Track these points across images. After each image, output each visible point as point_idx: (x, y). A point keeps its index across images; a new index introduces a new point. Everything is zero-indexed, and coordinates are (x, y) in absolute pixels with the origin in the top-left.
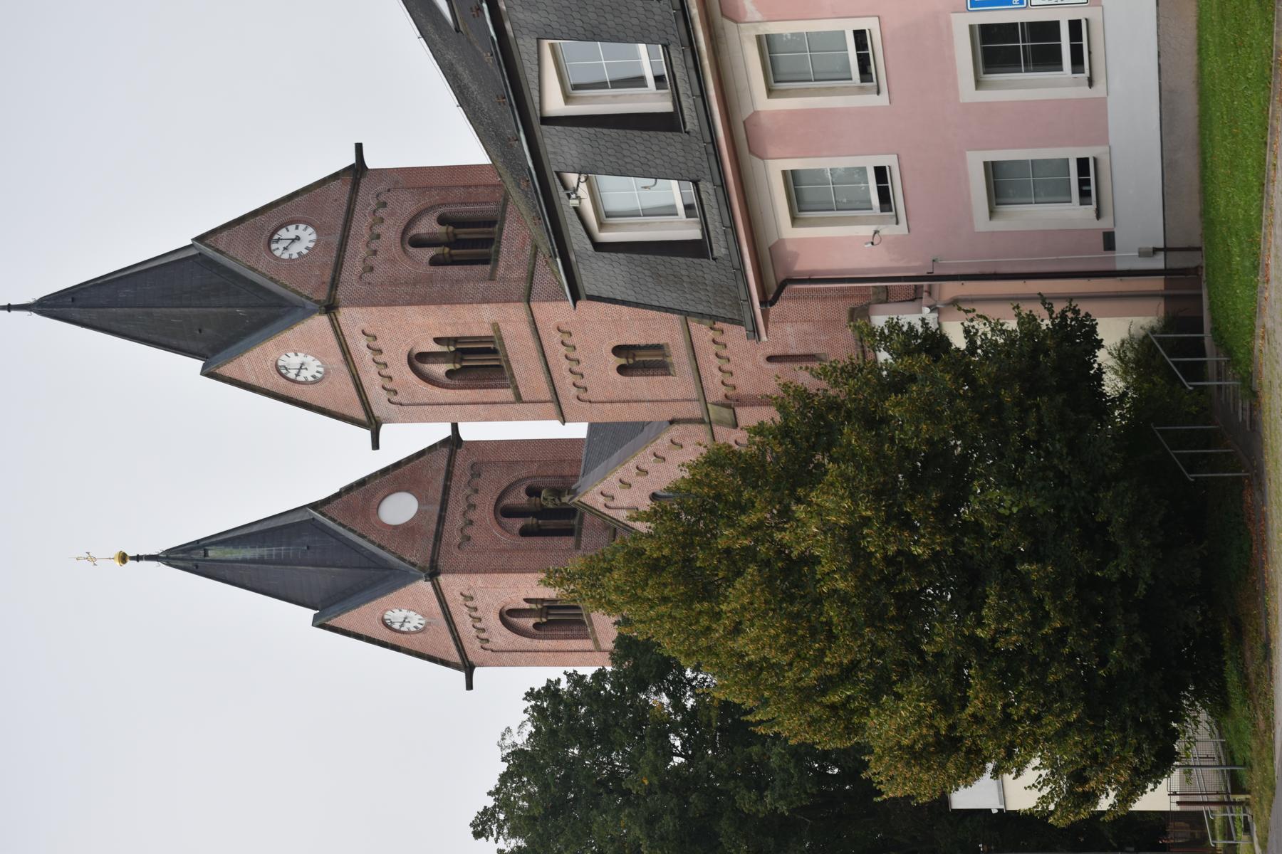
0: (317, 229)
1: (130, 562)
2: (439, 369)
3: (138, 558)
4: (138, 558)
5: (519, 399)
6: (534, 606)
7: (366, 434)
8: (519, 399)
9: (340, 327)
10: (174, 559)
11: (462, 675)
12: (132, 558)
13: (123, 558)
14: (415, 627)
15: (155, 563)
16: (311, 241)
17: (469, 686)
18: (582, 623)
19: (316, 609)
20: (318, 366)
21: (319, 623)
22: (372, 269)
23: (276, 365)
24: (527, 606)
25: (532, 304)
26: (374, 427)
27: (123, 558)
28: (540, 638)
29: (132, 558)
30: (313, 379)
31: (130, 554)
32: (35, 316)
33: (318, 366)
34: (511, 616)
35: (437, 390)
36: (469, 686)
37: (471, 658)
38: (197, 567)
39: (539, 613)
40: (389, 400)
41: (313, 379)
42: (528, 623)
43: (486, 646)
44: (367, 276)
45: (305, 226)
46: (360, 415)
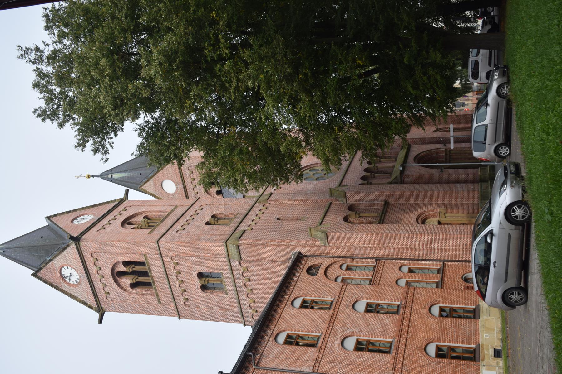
2: (126, 281)
20: (77, 279)
33: (77, 279)
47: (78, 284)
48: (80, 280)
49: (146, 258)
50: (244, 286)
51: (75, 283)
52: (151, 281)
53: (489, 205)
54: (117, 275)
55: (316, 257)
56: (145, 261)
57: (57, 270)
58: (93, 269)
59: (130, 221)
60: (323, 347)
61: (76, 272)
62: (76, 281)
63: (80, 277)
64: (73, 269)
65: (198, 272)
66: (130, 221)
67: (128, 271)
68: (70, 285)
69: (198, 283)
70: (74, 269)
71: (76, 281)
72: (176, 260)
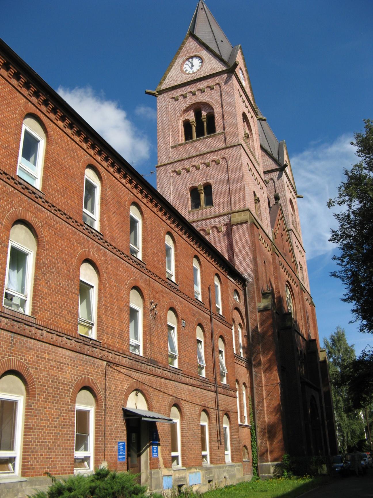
2: (191, 116)
47: (184, 73)
48: (189, 74)
49: (220, 134)
50: (16, 368)
51: (185, 70)
52: (193, 139)
53: (301, 337)
54: (197, 108)
55: (218, 406)
56: (217, 132)
57: (197, 53)
58: (202, 85)
59: (301, 482)
60: (166, 285)
61: (196, 70)
62: (187, 70)
63: (191, 74)
64: (200, 67)
65: (212, 183)
66: (301, 482)
67: (203, 118)
68: (182, 65)
69: (199, 183)
70: (201, 68)
71: (187, 70)
72: (222, 162)
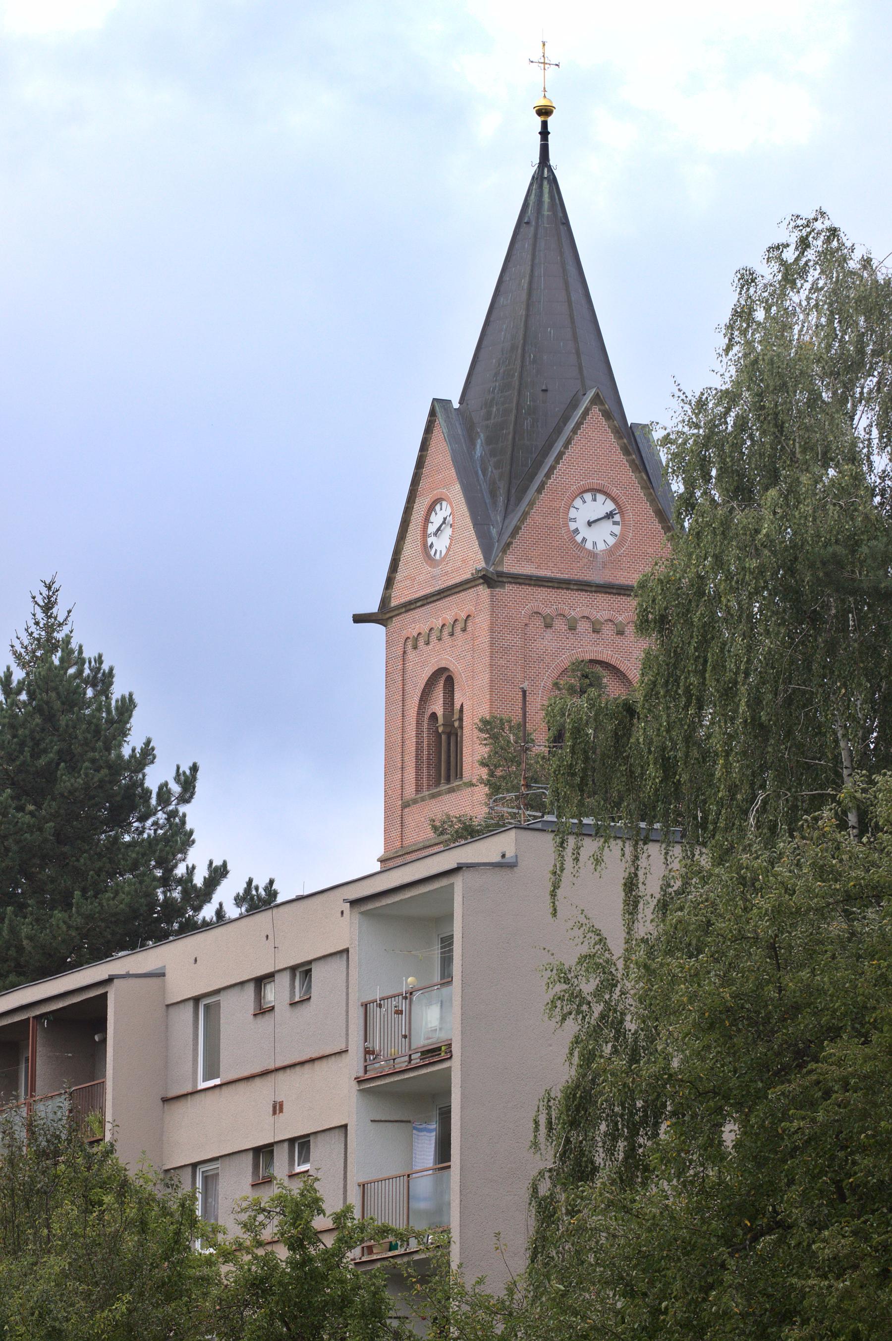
0: (611, 551)
1: (538, 120)
3: (544, 133)
4: (544, 133)
5: (405, 805)
6: (456, 716)
7: (373, 607)
8: (405, 805)
9: (473, 587)
10: (541, 187)
11: (373, 607)
12: (545, 124)
13: (544, 112)
14: (432, 546)
15: (537, 160)
16: (595, 544)
17: (359, 619)
18: (438, 783)
19: (461, 402)
21: (438, 407)
22: (548, 626)
23: (442, 499)
24: (457, 706)
25: (514, 831)
26: (380, 617)
27: (544, 112)
28: (419, 724)
29: (545, 124)
30: (429, 544)
31: (550, 120)
32: (531, 170)
34: (446, 680)
35: (416, 699)
36: (359, 619)
37: (396, 622)
38: (527, 223)
39: (448, 724)
40: (408, 638)
41: (429, 544)
42: (437, 706)
43: (410, 644)
44: (539, 623)
45: (618, 533)
46: (400, 596)
